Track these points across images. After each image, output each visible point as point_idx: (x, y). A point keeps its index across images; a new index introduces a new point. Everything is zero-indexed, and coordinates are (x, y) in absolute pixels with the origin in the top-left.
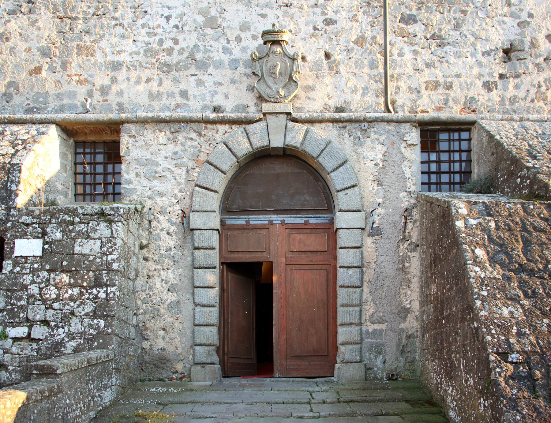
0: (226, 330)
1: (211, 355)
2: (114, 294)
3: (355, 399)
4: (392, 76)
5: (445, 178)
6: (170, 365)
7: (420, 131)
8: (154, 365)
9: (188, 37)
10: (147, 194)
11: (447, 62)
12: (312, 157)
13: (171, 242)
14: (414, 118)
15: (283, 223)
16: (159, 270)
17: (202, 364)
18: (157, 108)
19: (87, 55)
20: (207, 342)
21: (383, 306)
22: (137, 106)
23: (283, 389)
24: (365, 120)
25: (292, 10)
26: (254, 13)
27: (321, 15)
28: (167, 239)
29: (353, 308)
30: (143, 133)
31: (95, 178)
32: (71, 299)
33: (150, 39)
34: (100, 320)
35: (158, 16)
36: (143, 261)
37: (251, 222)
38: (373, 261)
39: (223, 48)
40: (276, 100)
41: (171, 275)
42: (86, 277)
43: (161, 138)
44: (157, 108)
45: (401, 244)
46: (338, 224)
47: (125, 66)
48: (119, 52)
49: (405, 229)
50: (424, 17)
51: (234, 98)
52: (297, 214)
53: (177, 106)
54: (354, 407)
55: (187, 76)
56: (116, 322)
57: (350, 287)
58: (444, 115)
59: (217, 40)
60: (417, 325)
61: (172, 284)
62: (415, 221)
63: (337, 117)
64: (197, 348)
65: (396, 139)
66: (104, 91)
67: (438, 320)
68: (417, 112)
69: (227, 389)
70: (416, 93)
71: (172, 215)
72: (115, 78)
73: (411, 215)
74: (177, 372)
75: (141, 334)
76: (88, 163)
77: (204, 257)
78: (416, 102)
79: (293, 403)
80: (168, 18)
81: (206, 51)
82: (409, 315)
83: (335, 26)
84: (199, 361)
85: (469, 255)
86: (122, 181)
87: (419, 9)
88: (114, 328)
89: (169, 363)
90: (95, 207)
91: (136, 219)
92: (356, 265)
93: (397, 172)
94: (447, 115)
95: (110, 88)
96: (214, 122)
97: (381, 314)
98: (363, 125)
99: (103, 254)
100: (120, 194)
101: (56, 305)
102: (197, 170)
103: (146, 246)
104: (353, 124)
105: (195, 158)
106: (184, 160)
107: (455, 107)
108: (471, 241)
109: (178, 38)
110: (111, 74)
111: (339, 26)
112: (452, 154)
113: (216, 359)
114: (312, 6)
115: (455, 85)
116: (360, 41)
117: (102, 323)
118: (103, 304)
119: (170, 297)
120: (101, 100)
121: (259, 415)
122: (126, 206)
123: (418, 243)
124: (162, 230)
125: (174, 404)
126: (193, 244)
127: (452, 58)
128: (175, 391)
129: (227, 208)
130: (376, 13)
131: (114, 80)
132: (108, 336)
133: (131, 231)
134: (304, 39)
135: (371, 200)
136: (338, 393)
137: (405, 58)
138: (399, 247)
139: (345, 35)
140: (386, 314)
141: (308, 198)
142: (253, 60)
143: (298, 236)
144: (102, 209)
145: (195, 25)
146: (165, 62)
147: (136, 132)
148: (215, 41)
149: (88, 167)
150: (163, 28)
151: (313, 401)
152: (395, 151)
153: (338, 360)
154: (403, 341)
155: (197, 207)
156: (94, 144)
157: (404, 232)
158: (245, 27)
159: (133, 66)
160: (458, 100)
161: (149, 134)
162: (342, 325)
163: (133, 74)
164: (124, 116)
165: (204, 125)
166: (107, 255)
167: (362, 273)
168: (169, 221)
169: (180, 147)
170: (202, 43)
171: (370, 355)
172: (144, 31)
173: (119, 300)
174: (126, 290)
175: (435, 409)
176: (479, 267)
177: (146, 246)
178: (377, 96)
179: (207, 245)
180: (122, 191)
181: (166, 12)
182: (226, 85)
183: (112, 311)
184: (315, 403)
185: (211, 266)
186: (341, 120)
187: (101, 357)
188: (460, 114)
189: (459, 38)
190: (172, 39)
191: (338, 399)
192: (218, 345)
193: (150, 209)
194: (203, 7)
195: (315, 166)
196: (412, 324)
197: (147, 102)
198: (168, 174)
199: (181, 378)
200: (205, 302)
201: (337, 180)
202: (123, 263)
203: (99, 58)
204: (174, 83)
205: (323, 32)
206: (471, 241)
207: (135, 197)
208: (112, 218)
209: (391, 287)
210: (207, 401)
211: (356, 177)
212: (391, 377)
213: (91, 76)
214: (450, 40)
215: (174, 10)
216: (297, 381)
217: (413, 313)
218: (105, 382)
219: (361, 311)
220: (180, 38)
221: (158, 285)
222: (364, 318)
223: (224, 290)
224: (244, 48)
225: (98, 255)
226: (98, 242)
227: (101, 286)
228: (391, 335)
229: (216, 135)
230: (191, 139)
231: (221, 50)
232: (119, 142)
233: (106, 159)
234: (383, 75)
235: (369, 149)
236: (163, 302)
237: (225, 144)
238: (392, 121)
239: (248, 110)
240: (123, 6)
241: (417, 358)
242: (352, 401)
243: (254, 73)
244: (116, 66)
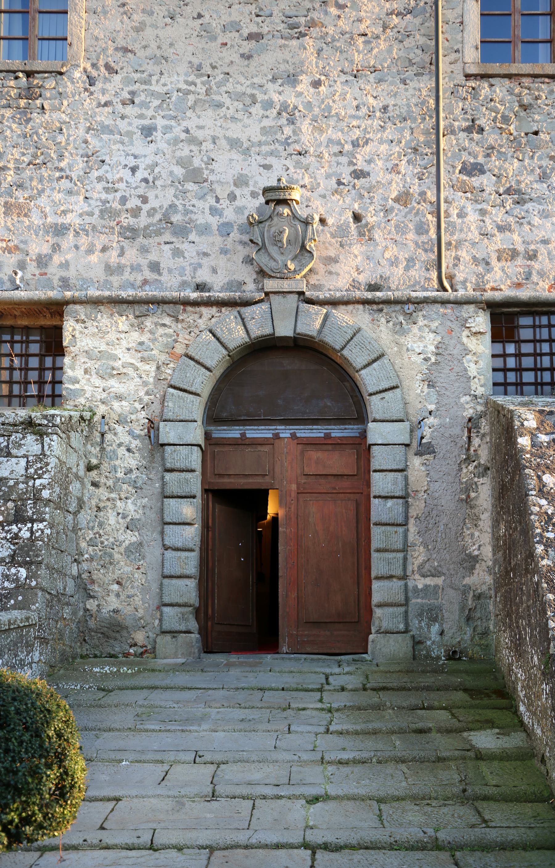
0: (210, 584)
1: (186, 620)
2: (43, 532)
3: (389, 685)
4: (449, 244)
5: (529, 377)
6: (126, 635)
7: (491, 314)
8: (102, 633)
9: (161, 194)
10: (99, 397)
11: (529, 223)
12: (334, 349)
13: (132, 461)
14: (479, 298)
15: (293, 436)
16: (113, 500)
17: (173, 632)
18: (116, 284)
19: (19, 215)
20: (181, 601)
21: (438, 552)
22: (87, 282)
23: (287, 670)
24: (409, 301)
25: (309, 160)
26: (254, 164)
27: (349, 165)
28: (127, 457)
29: (394, 554)
30: (96, 317)
31: (26, 375)
33: (108, 196)
34: (19, 569)
35: (120, 167)
36: (91, 488)
37: (248, 436)
38: (423, 489)
39: (211, 208)
40: (283, 276)
41: (131, 507)
42: (3, 509)
43: (121, 324)
44: (116, 284)
45: (463, 466)
46: (372, 438)
47: (72, 230)
48: (64, 212)
49: (469, 446)
50: (495, 166)
51: (224, 272)
52: (313, 425)
53: (145, 282)
54: (385, 697)
55: (159, 244)
56: (43, 572)
57: (389, 525)
58: (524, 294)
59: (202, 197)
60: (489, 579)
61: (132, 519)
62: (484, 435)
63: (370, 297)
64: (166, 609)
65: (455, 326)
66: (42, 261)
67: (507, 573)
68: (485, 290)
69: (205, 669)
70: (484, 265)
71: (134, 425)
72: (58, 245)
73: (477, 427)
74: (135, 645)
75: (85, 589)
76: (16, 355)
77: (179, 482)
78: (483, 277)
79: (297, 690)
80: (134, 170)
81: (187, 212)
82: (477, 566)
83: (368, 180)
84: (169, 629)
85: (533, 483)
86: (64, 379)
87: (488, 155)
88: (39, 580)
89: (125, 631)
90: (22, 413)
91: (82, 431)
92: (397, 494)
93: (456, 369)
94: (528, 294)
95: (51, 258)
96: (195, 304)
97: (436, 564)
98: (406, 307)
99: (29, 477)
100: (60, 396)
102: (172, 365)
103: (97, 467)
104: (393, 306)
105: (170, 350)
106: (153, 352)
107: (541, 283)
108: (539, 464)
109: (147, 195)
110: (52, 240)
111: (373, 179)
112: (538, 345)
113: (193, 625)
114: (335, 155)
115: (541, 254)
116: (403, 198)
117: (23, 573)
118: (26, 545)
119: (129, 537)
120: (37, 272)
121: (243, 705)
122: (66, 413)
123: (489, 465)
124: (120, 445)
125: (123, 689)
126: (164, 465)
127: (537, 219)
128: (130, 671)
129: (215, 415)
130: (425, 161)
131: (56, 248)
132: (30, 591)
133: (73, 446)
134: (324, 197)
135: (420, 406)
136: (367, 677)
137: (466, 218)
138: (460, 470)
139: (381, 191)
140: (442, 563)
141: (329, 404)
142: (251, 224)
143: (314, 455)
144: (30, 417)
145: (171, 179)
146: (129, 225)
147: (86, 315)
148: (200, 199)
149: (16, 361)
150: (127, 182)
151: (326, 687)
152: (453, 342)
153: (373, 630)
154: (470, 603)
155: (169, 415)
156: (27, 330)
157: (468, 449)
158: (241, 181)
159: (83, 230)
160: (545, 273)
161: (104, 319)
162: (378, 578)
163: (84, 241)
164: (68, 294)
165: (182, 307)
166: (34, 479)
167: (407, 506)
168: (130, 433)
169: (149, 335)
170: (181, 201)
171: (420, 622)
172: (99, 186)
173: (49, 540)
174: (62, 527)
175: (503, 702)
176: (546, 499)
177: (97, 467)
178: (428, 270)
179: (183, 466)
180: (64, 393)
181: (132, 162)
182: (213, 256)
183: (37, 556)
184: (330, 690)
185: (188, 494)
186: (376, 300)
187: (15, 621)
188: (549, 291)
189: (547, 193)
190: (139, 197)
191: (364, 685)
192: (197, 605)
193: (103, 417)
194: (183, 155)
195: (339, 361)
196: (482, 578)
197: (103, 277)
198: (130, 371)
199: (142, 654)
200: (180, 545)
201: (370, 379)
202: (57, 490)
203: (36, 219)
204: (141, 253)
205: (350, 188)
206: (539, 464)
207: (82, 401)
208: (44, 429)
209: (450, 525)
210: (172, 685)
211: (398, 376)
212: (453, 656)
213: (25, 242)
214: (533, 195)
215: (143, 159)
216: (312, 659)
217: (483, 563)
218: (22, 656)
219: (405, 559)
220: (151, 195)
221: (112, 520)
222: (410, 568)
223: (208, 527)
224: (239, 208)
225: (21, 479)
226: (23, 462)
227: (24, 522)
228: (451, 593)
229: (200, 321)
230: (164, 325)
231: (207, 211)
232: (61, 328)
233: (43, 350)
234: (436, 242)
235: (416, 339)
236: (118, 543)
237: (211, 331)
238: (448, 302)
239: (244, 287)
240: (71, 154)
241: (491, 627)
242: (384, 689)
243: (251, 241)
244: (60, 230)
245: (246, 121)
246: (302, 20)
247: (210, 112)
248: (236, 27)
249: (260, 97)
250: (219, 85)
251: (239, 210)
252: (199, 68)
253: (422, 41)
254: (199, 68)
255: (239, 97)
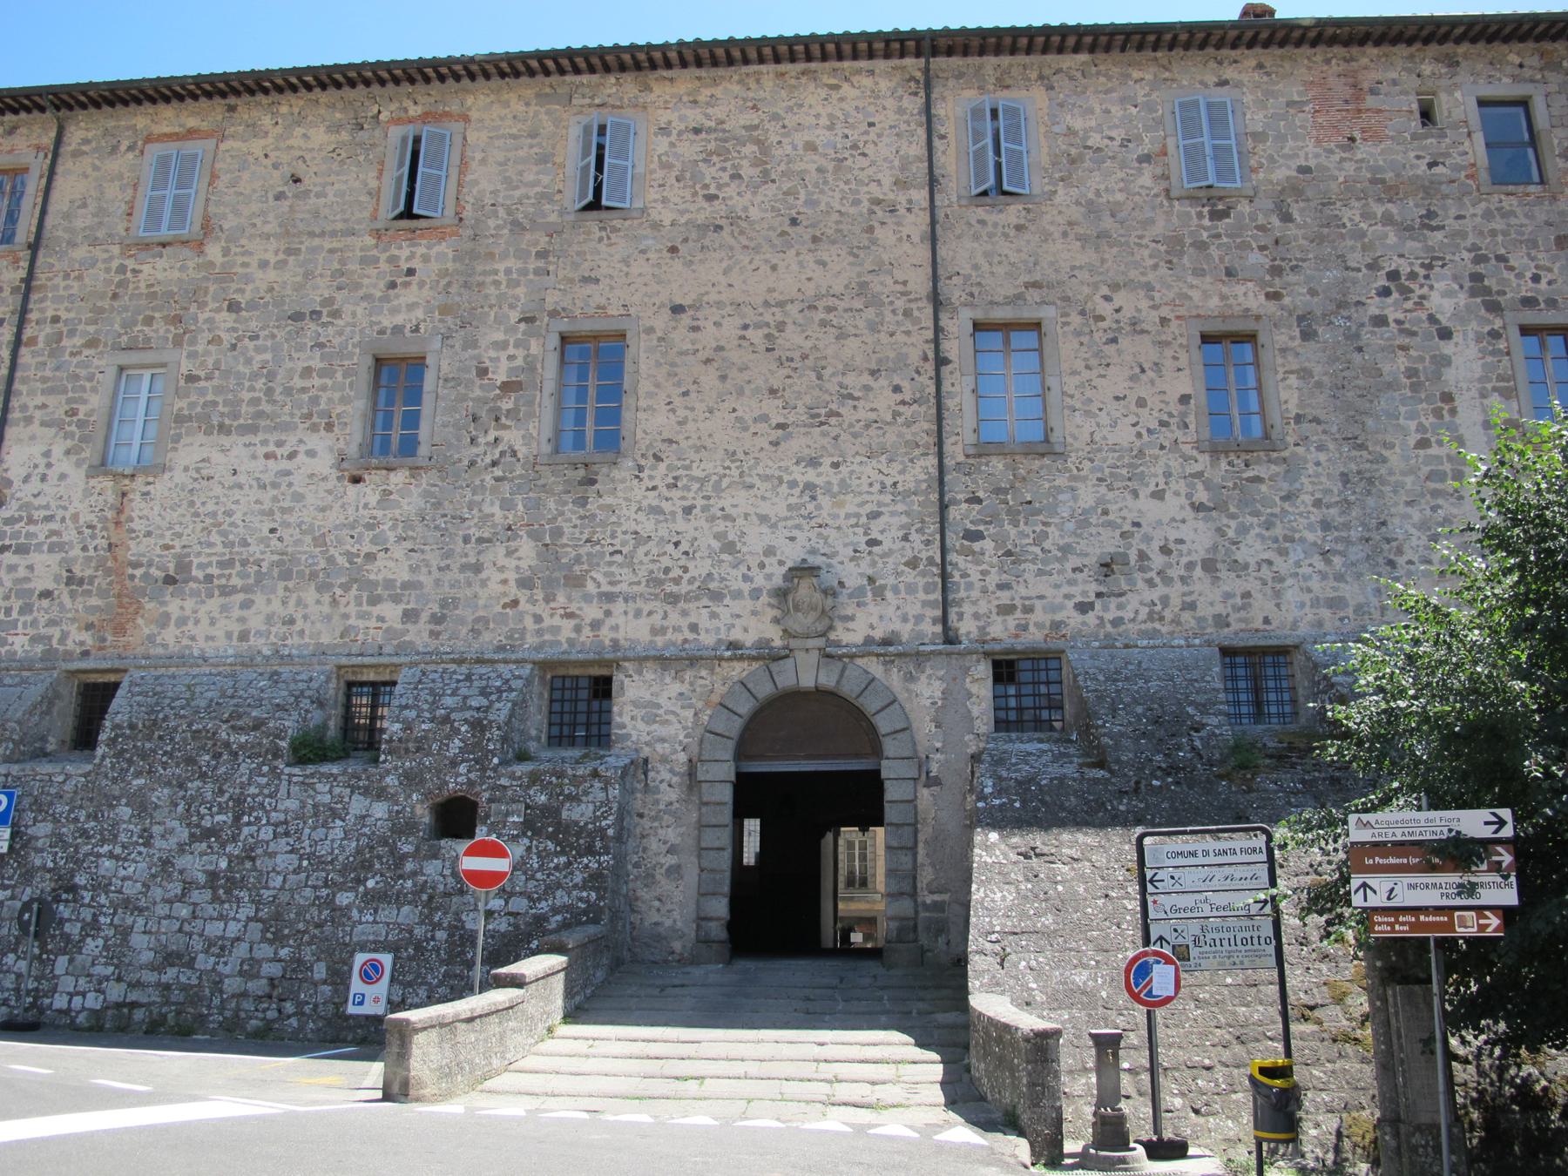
13: (673, 795)
32: (557, 868)
59: (735, 567)
66: (596, 625)
80: (677, 544)
81: (723, 579)
99: (596, 819)
101: (539, 876)
158: (770, 551)
167: (916, 832)
168: (671, 771)
203: (591, 587)
220: (691, 565)
226: (591, 807)
244: (610, 597)
245: (775, 500)
246: (823, 411)
247: (743, 493)
248: (764, 418)
249: (786, 478)
250: (750, 468)
251: (769, 577)
252: (734, 453)
253: (926, 426)
254: (734, 453)
255: (766, 478)
